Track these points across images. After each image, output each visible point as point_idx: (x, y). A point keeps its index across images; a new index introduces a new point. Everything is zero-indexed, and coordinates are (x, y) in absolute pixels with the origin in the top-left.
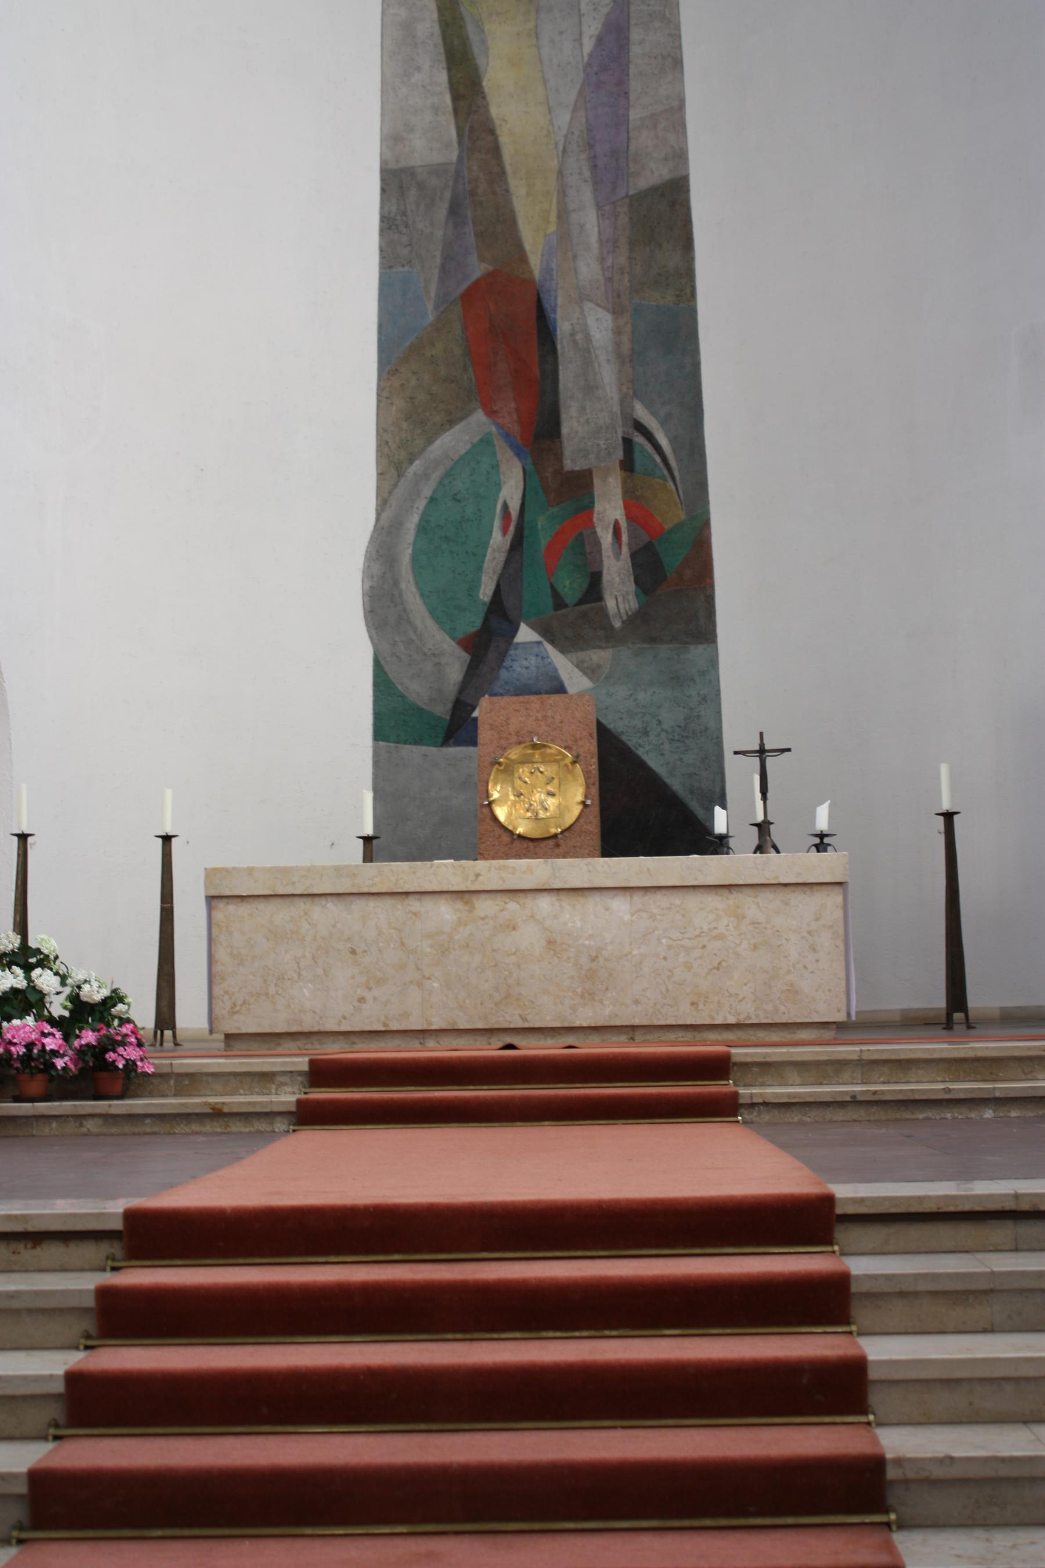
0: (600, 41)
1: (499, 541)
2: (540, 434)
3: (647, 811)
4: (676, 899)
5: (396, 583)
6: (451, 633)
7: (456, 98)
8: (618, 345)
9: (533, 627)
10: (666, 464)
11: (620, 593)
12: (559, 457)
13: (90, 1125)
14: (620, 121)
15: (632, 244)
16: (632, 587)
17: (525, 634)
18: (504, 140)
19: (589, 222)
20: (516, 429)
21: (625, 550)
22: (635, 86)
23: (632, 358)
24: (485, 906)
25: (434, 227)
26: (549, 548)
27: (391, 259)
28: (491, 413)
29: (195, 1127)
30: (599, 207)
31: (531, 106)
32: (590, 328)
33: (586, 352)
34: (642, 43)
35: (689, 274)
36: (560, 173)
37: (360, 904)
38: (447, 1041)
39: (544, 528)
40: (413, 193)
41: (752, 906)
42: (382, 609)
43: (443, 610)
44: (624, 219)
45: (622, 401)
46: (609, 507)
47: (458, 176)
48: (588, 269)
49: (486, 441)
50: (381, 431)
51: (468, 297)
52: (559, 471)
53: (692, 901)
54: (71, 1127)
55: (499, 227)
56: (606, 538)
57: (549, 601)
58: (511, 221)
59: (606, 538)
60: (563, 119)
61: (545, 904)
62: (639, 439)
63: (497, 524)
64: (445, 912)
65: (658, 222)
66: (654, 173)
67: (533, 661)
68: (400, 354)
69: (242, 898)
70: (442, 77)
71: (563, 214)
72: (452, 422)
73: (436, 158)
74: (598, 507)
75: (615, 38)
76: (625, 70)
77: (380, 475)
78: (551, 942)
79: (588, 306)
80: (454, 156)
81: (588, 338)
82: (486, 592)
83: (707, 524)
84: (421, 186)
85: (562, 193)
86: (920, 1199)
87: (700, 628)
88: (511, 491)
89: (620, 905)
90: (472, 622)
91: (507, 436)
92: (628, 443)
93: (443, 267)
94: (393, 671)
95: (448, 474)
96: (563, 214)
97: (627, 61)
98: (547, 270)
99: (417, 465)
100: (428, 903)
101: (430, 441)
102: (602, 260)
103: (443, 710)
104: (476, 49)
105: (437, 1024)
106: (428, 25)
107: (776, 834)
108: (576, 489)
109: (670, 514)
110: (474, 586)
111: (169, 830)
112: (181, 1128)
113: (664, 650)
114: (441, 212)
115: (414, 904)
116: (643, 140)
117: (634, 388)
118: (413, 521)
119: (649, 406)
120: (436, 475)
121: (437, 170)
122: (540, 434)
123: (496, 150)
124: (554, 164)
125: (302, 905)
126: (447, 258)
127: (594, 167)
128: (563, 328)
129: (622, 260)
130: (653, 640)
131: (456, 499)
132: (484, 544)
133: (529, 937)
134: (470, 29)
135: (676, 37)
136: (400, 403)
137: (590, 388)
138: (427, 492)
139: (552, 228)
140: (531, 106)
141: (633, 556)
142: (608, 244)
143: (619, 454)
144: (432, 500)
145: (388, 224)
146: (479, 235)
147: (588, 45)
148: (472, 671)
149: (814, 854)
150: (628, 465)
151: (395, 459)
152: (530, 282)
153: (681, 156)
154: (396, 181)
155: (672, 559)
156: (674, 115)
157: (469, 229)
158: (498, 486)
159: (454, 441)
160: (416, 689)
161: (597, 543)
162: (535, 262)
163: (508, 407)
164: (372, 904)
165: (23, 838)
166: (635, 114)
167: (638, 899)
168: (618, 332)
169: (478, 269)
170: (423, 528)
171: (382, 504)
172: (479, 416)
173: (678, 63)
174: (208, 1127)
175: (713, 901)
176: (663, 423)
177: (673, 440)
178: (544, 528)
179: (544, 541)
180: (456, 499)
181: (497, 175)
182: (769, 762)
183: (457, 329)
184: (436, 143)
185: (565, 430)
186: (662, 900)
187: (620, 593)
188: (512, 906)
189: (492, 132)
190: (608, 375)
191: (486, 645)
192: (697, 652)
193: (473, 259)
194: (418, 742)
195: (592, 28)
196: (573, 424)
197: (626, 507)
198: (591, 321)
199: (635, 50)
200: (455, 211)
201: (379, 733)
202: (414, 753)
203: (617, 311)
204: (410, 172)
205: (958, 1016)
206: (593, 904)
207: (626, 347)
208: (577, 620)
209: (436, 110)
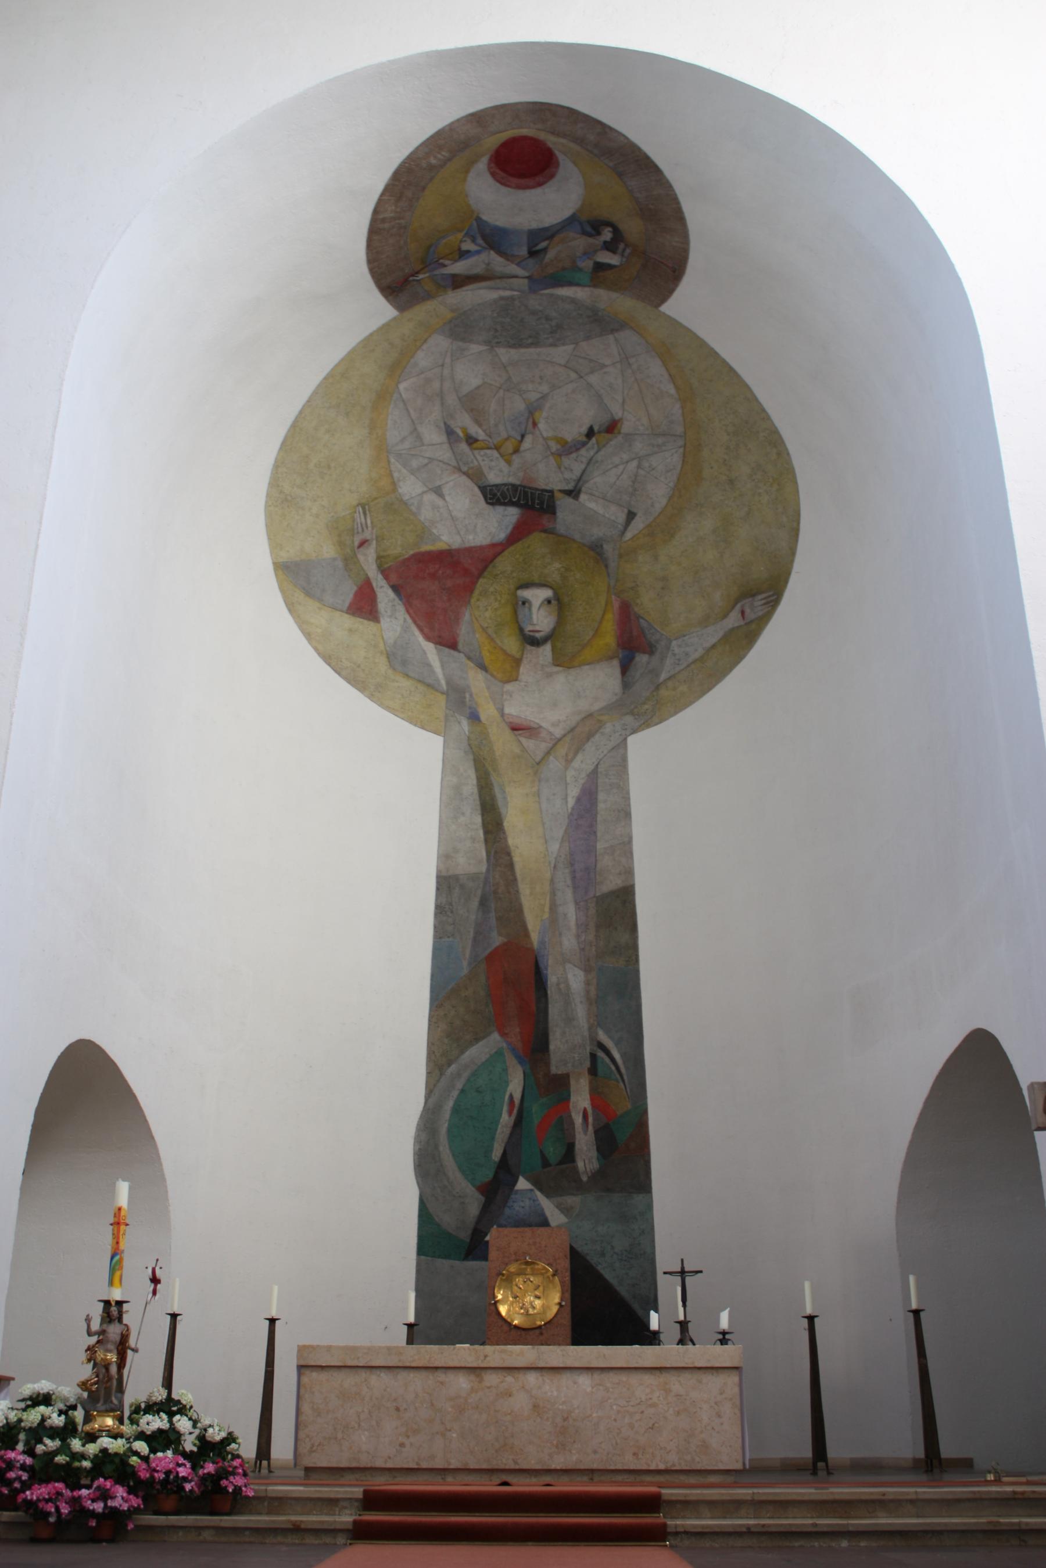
0: (578, 800)
1: (506, 1120)
2: (535, 1048)
3: (605, 1311)
4: (623, 1377)
5: (436, 1147)
7: (486, 832)
8: (588, 992)
9: (527, 1179)
10: (618, 1071)
11: (587, 1157)
12: (548, 1064)
13: (207, 1535)
14: (590, 850)
15: (598, 927)
16: (594, 1153)
18: (516, 859)
19: (570, 912)
21: (590, 1128)
22: (600, 828)
28: (503, 1034)
30: (577, 903)
31: (534, 837)
32: (569, 980)
33: (567, 996)
34: (605, 802)
35: (635, 947)
36: (552, 881)
37: (403, 1375)
39: (537, 1112)
40: (457, 891)
41: (677, 1384)
42: (426, 1164)
45: (590, 1029)
46: (581, 1099)
47: (486, 881)
48: (569, 942)
49: (499, 1053)
50: (430, 1044)
51: (491, 958)
53: (634, 1379)
55: (511, 914)
56: (578, 1120)
58: (520, 911)
59: (578, 1120)
60: (555, 847)
61: (532, 1378)
62: (601, 1054)
63: (505, 1108)
64: (462, 1383)
65: (614, 914)
66: (612, 883)
67: (527, 1203)
68: (443, 994)
69: (322, 1367)
70: (478, 819)
71: (553, 907)
72: (477, 1040)
74: (573, 1098)
75: (588, 798)
77: (429, 1073)
78: (535, 1407)
79: (568, 966)
80: (484, 868)
81: (568, 987)
82: (496, 1154)
83: (645, 1112)
84: (462, 887)
85: (553, 893)
88: (515, 1087)
89: (585, 1381)
90: (486, 1174)
91: (513, 1050)
92: (593, 1057)
95: (475, 1074)
96: (553, 907)
98: (542, 943)
100: (450, 1377)
101: (462, 1052)
102: (578, 936)
104: (500, 802)
105: (455, 1464)
106: (470, 787)
108: (557, 1087)
109: (622, 1105)
111: (274, 1314)
114: (475, 903)
115: (441, 1376)
116: (605, 862)
118: (450, 1104)
119: (607, 1032)
120: (466, 1075)
121: (474, 877)
123: (511, 866)
124: (548, 875)
125: (364, 1374)
126: (477, 933)
127: (574, 878)
128: (552, 980)
130: (608, 1190)
133: (520, 1402)
134: (497, 790)
135: (627, 798)
137: (570, 1020)
138: (459, 1085)
139: (546, 916)
140: (534, 837)
141: (596, 1132)
143: (588, 1064)
144: (462, 1091)
145: (440, 910)
147: (571, 802)
149: (719, 1347)
150: (593, 1071)
151: (438, 1063)
152: (533, 950)
153: (629, 872)
154: (446, 883)
156: (626, 846)
157: (493, 915)
158: (507, 1083)
159: (478, 1052)
160: (448, 1220)
161: (572, 1123)
162: (535, 937)
164: (412, 1375)
166: (600, 846)
167: (597, 1376)
168: (588, 983)
170: (456, 1110)
172: (496, 1036)
173: (628, 815)
175: (648, 1379)
176: (617, 1044)
177: (623, 1055)
178: (537, 1112)
179: (536, 1121)
180: (478, 1091)
181: (511, 881)
184: (472, 859)
185: (552, 1047)
187: (587, 1157)
189: (509, 854)
190: (581, 1011)
191: (496, 1189)
192: (638, 1198)
193: (494, 934)
194: (447, 1257)
195: (574, 792)
196: (558, 1043)
197: (592, 1099)
198: (570, 976)
199: (601, 806)
200: (483, 902)
201: (421, 1250)
203: (587, 970)
204: (456, 878)
206: (565, 1379)
208: (557, 1176)
209: (473, 840)
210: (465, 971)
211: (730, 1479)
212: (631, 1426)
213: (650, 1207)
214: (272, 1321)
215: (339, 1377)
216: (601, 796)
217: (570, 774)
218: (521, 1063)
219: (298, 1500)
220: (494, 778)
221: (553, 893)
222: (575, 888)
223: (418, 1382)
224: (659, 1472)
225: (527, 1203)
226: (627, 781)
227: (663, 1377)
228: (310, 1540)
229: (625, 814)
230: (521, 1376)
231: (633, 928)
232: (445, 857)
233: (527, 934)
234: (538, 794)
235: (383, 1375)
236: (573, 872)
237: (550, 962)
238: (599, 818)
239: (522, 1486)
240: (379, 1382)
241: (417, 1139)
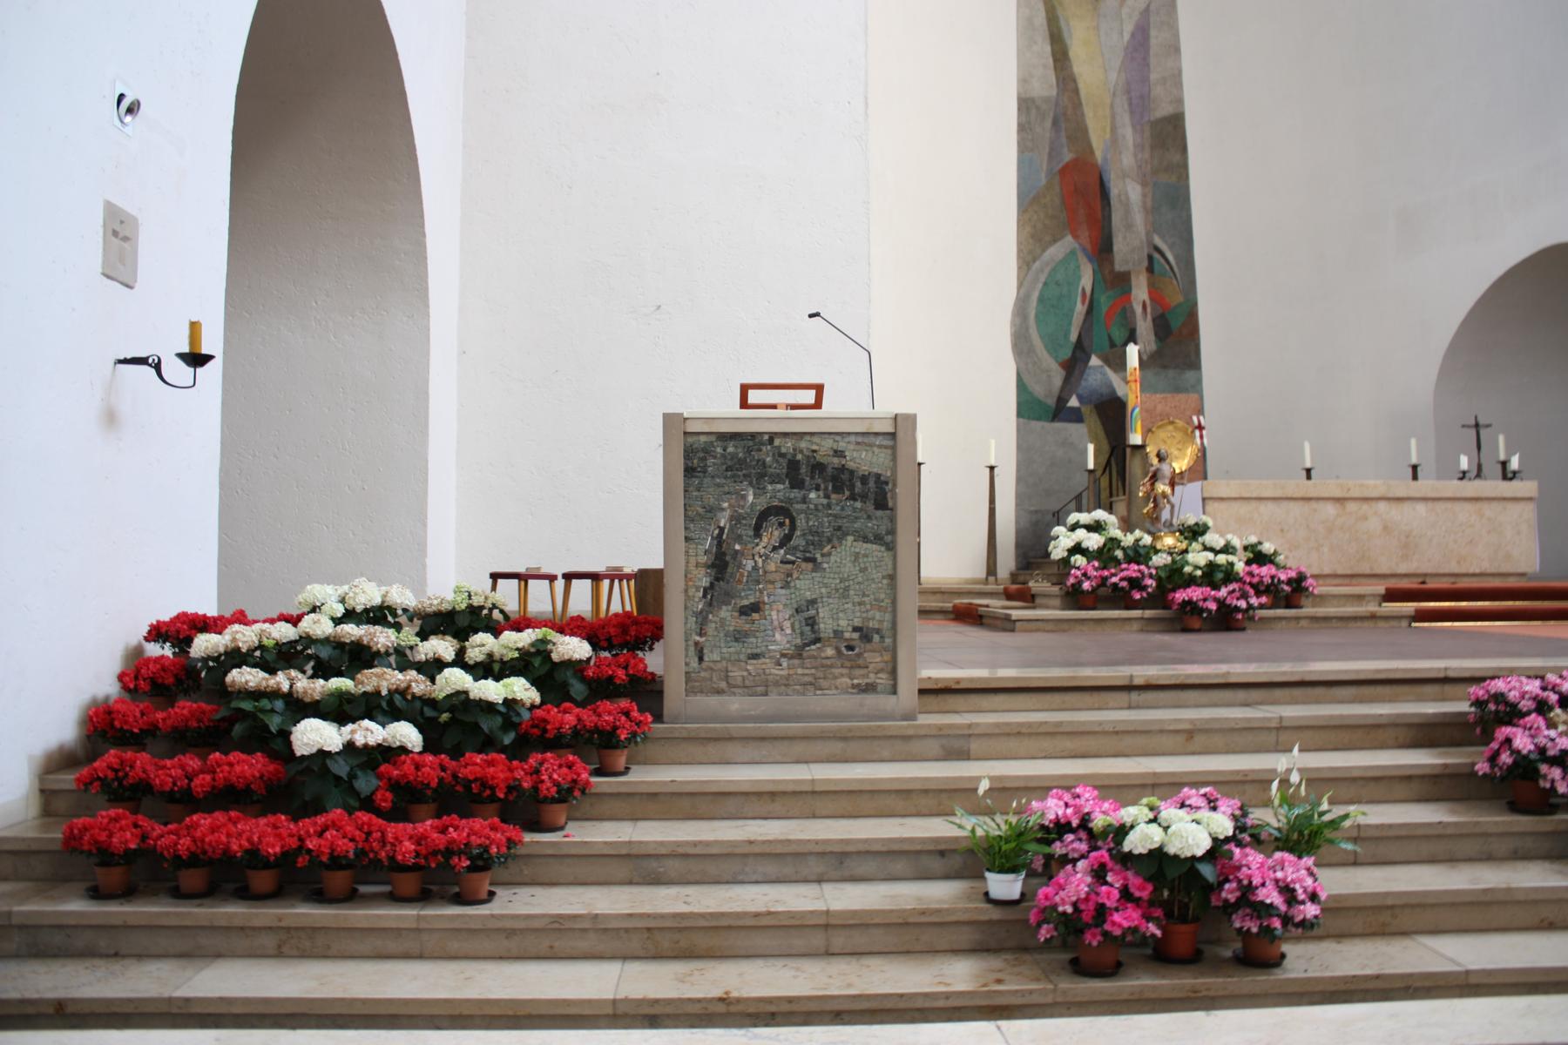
0: (1133, 35)
1: (1080, 309)
2: (1102, 250)
4: (1449, 505)
5: (1027, 329)
6: (1056, 359)
7: (1055, 61)
8: (1144, 203)
9: (1099, 357)
10: (1172, 268)
12: (1112, 263)
13: (1304, 623)
14: (1145, 80)
15: (1152, 148)
16: (1153, 338)
17: (1095, 361)
18: (1081, 86)
19: (1128, 134)
20: (1088, 247)
21: (1149, 317)
22: (1153, 61)
23: (1152, 211)
24: (1351, 506)
25: (1044, 130)
26: (1108, 313)
27: (1023, 148)
28: (1075, 237)
29: (1359, 624)
30: (1133, 126)
31: (1097, 69)
32: (1129, 194)
33: (1127, 205)
34: (1156, 38)
35: (1185, 166)
36: (1112, 106)
37: (1285, 504)
38: (1465, 579)
39: (1104, 303)
40: (1034, 111)
41: (1489, 510)
43: (1052, 345)
44: (1147, 134)
45: (1147, 234)
46: (1140, 292)
47: (1057, 104)
48: (1128, 160)
49: (1073, 252)
50: (1019, 243)
51: (1064, 171)
52: (1112, 271)
53: (1457, 506)
54: (1293, 624)
55: (1079, 134)
56: (1138, 310)
57: (1107, 343)
58: (1085, 131)
59: (1138, 310)
60: (1113, 76)
61: (1382, 506)
62: (1156, 256)
63: (1079, 299)
64: (1330, 510)
65: (1168, 135)
66: (1164, 110)
67: (1099, 376)
68: (1028, 202)
69: (1222, 499)
70: (1048, 49)
71: (1114, 129)
72: (1055, 241)
73: (1045, 93)
74: (1134, 292)
76: (1147, 51)
77: (1019, 268)
78: (1385, 528)
79: (1128, 181)
80: (1054, 93)
81: (1128, 198)
82: (1074, 337)
83: (1196, 304)
84: (1038, 108)
85: (1113, 117)
86: (1357, 671)
87: (1191, 361)
88: (1086, 281)
89: (1421, 508)
90: (1066, 353)
91: (1084, 250)
92: (1150, 258)
93: (1050, 155)
94: (1026, 379)
95: (1054, 270)
96: (1114, 129)
97: (1148, 47)
98: (1105, 159)
99: (1037, 264)
100: (1321, 505)
101: (1044, 251)
102: (1135, 155)
103: (1051, 402)
104: (1066, 35)
105: (1327, 571)
106: (1040, 19)
107: (1313, 473)
108: (1121, 282)
109: (1175, 298)
110: (1067, 334)
111: (993, 463)
112: (1352, 624)
113: (1171, 373)
114: (1048, 123)
115: (1314, 505)
116: (1158, 91)
117: (1154, 228)
118: (1035, 295)
119: (1162, 237)
120: (1047, 271)
121: (1047, 100)
122: (1102, 250)
123: (1076, 91)
124: (1108, 101)
125: (1254, 504)
126: (1051, 149)
127: (1130, 104)
128: (1114, 192)
129: (1147, 155)
130: (1165, 367)
131: (1057, 283)
132: (1072, 310)
133: (1374, 524)
134: (1063, 24)
135: (1176, 36)
136: (1028, 229)
137: (1129, 226)
138: (1043, 278)
139: (1108, 136)
140: (1097, 69)
141: (1154, 320)
142: (1139, 147)
143: (1146, 263)
144: (1045, 284)
145: (1022, 128)
146: (1068, 137)
147: (1127, 37)
148: (1067, 380)
149: (1456, 482)
150: (1150, 269)
151: (1026, 260)
152: (1095, 165)
153: (1180, 101)
154: (1025, 104)
155: (1176, 323)
156: (1176, 78)
157: (1063, 134)
158: (1080, 278)
159: (1057, 251)
160: (1038, 390)
161: (1133, 312)
162: (1099, 155)
163: (1085, 234)
164: (1292, 504)
165: (992, 468)
166: (1153, 76)
167: (1430, 504)
168: (1144, 195)
169: (1067, 156)
170: (1041, 300)
171: (1020, 285)
172: (1069, 238)
173: (1177, 50)
174: (1366, 624)
175: (1468, 506)
176: (1171, 247)
177: (1176, 257)
178: (1104, 303)
179: (1104, 309)
180: (1057, 283)
181: (1077, 105)
182: (1482, 432)
183: (1057, 188)
184: (1045, 85)
185: (1115, 248)
186: (1440, 506)
188: (1365, 506)
189: (1074, 81)
190: (1139, 219)
191: (1074, 365)
192: (1190, 375)
193: (1065, 150)
194: (1039, 419)
195: (1128, 28)
196: (1120, 246)
197: (1150, 293)
198: (1129, 189)
199: (1153, 41)
200: (1055, 123)
201: (1020, 414)
202: (1038, 425)
203: (1144, 184)
204: (1032, 100)
205: (991, 579)
206: (1406, 506)
207: (1149, 204)
209: (1045, 66)
210: (1044, 181)
211: (1347, 581)
212: (1455, 541)
213: (1199, 381)
214: (992, 468)
215: (1235, 506)
216: (1153, 33)
217: (1125, 11)
218: (1090, 260)
219: (1334, 596)
220: (1060, 12)
221: (1113, 117)
222: (1132, 112)
223: (1296, 509)
224: (1474, 575)
225: (1099, 376)
226: (1176, 20)
227: (1479, 505)
228: (1381, 624)
229: (1175, 49)
230: (1373, 504)
231: (1184, 149)
232: (1023, 81)
233: (1092, 152)
234: (1097, 28)
235: (1270, 506)
236: (1130, 99)
237: (1113, 176)
238: (1152, 52)
239: (1432, 584)
240: (1267, 509)
241: (1013, 324)
